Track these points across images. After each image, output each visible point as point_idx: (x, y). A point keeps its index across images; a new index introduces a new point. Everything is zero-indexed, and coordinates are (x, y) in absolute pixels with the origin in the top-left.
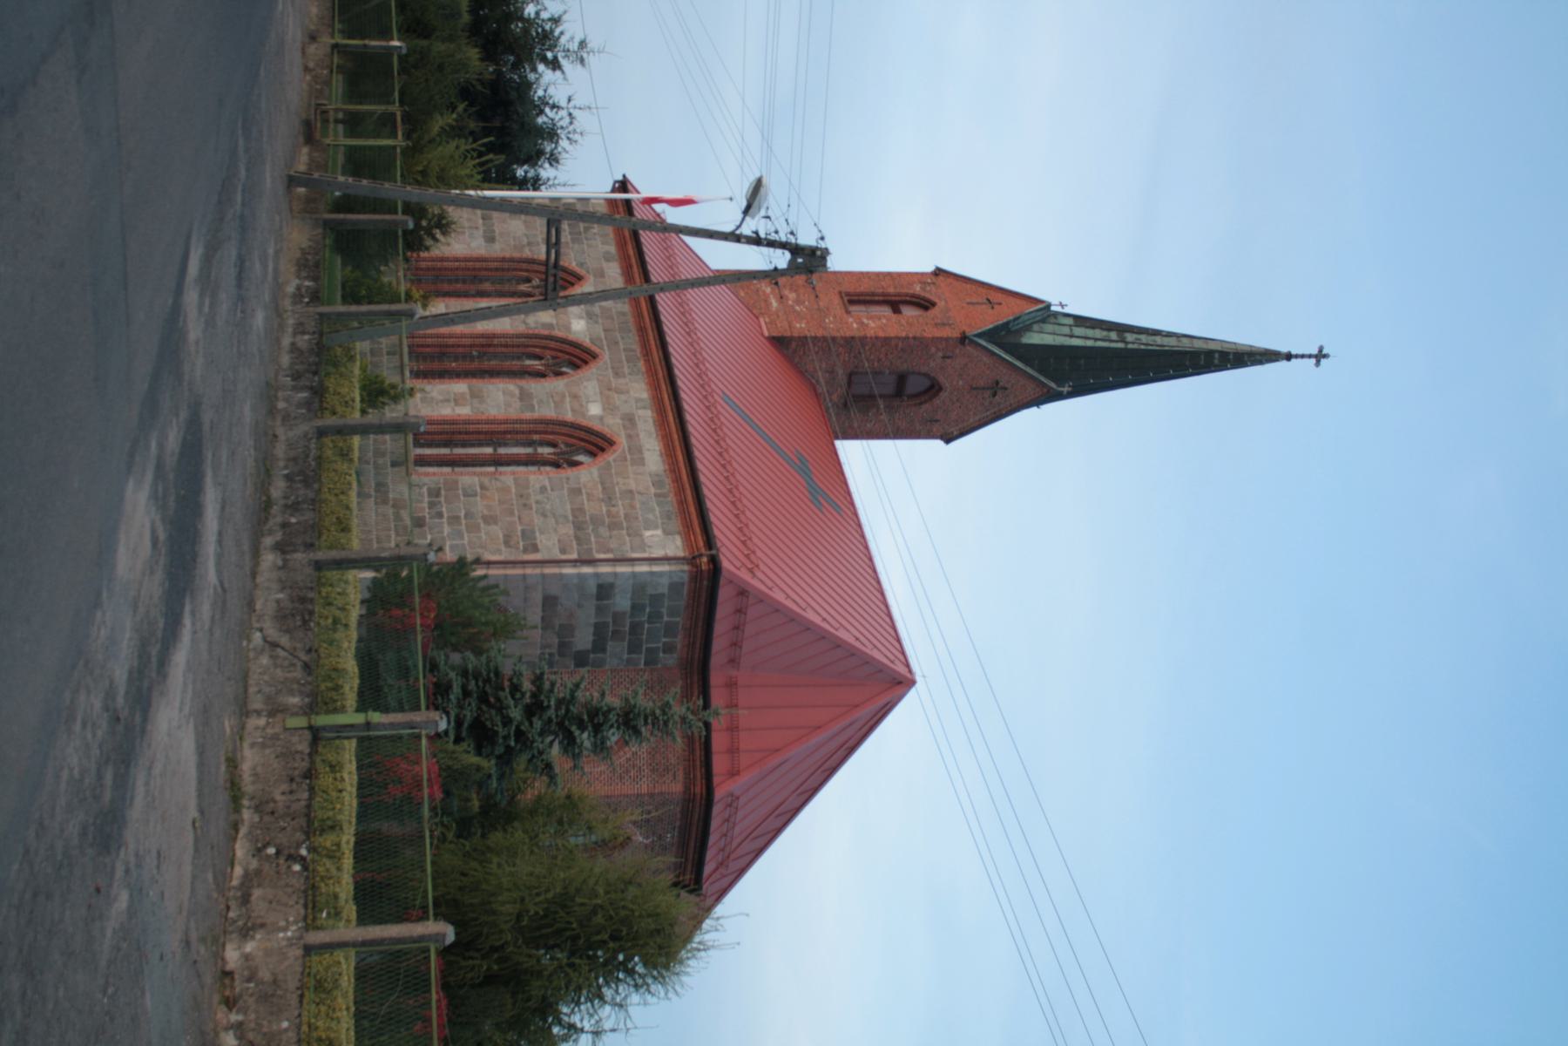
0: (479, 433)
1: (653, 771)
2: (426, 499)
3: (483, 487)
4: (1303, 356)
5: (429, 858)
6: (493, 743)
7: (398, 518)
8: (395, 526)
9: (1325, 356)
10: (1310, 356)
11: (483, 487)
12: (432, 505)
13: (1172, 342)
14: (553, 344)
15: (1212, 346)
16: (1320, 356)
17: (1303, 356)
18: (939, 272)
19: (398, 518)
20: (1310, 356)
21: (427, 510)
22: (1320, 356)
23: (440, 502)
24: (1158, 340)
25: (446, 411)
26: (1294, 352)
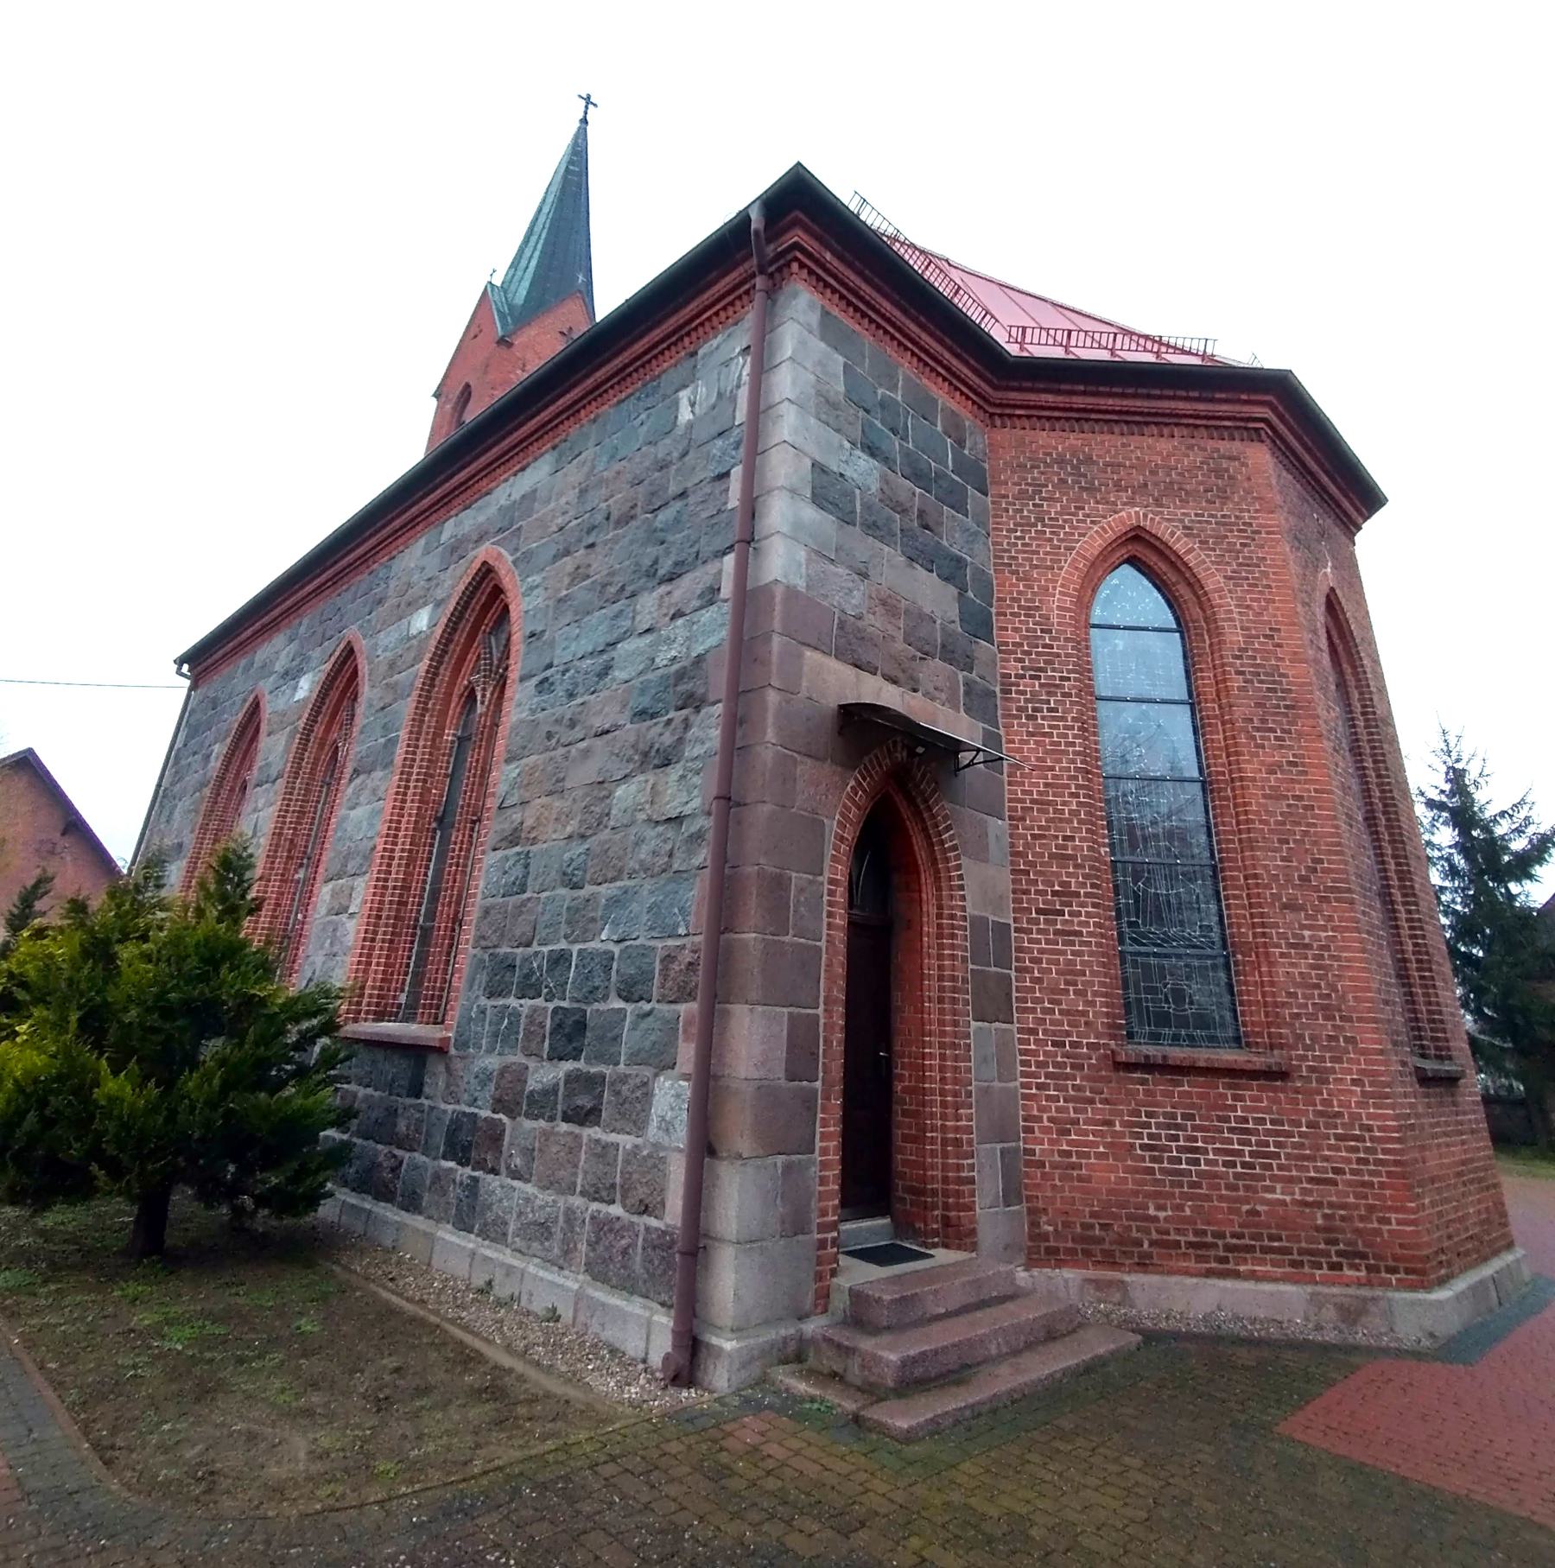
0: (411, 861)
1: (1225, 499)
2: (513, 1002)
3: (513, 839)
4: (586, 113)
5: (822, 994)
6: (198, 1068)
7: (540, 1104)
8: (566, 1118)
9: (589, 97)
10: (587, 107)
11: (513, 839)
12: (529, 988)
13: (550, 199)
14: (319, 729)
15: (562, 170)
16: (588, 99)
17: (586, 113)
18: (437, 395)
19: (540, 1104)
20: (587, 107)
21: (539, 1002)
22: (588, 99)
23: (526, 960)
24: (546, 210)
25: (352, 929)
26: (581, 116)
